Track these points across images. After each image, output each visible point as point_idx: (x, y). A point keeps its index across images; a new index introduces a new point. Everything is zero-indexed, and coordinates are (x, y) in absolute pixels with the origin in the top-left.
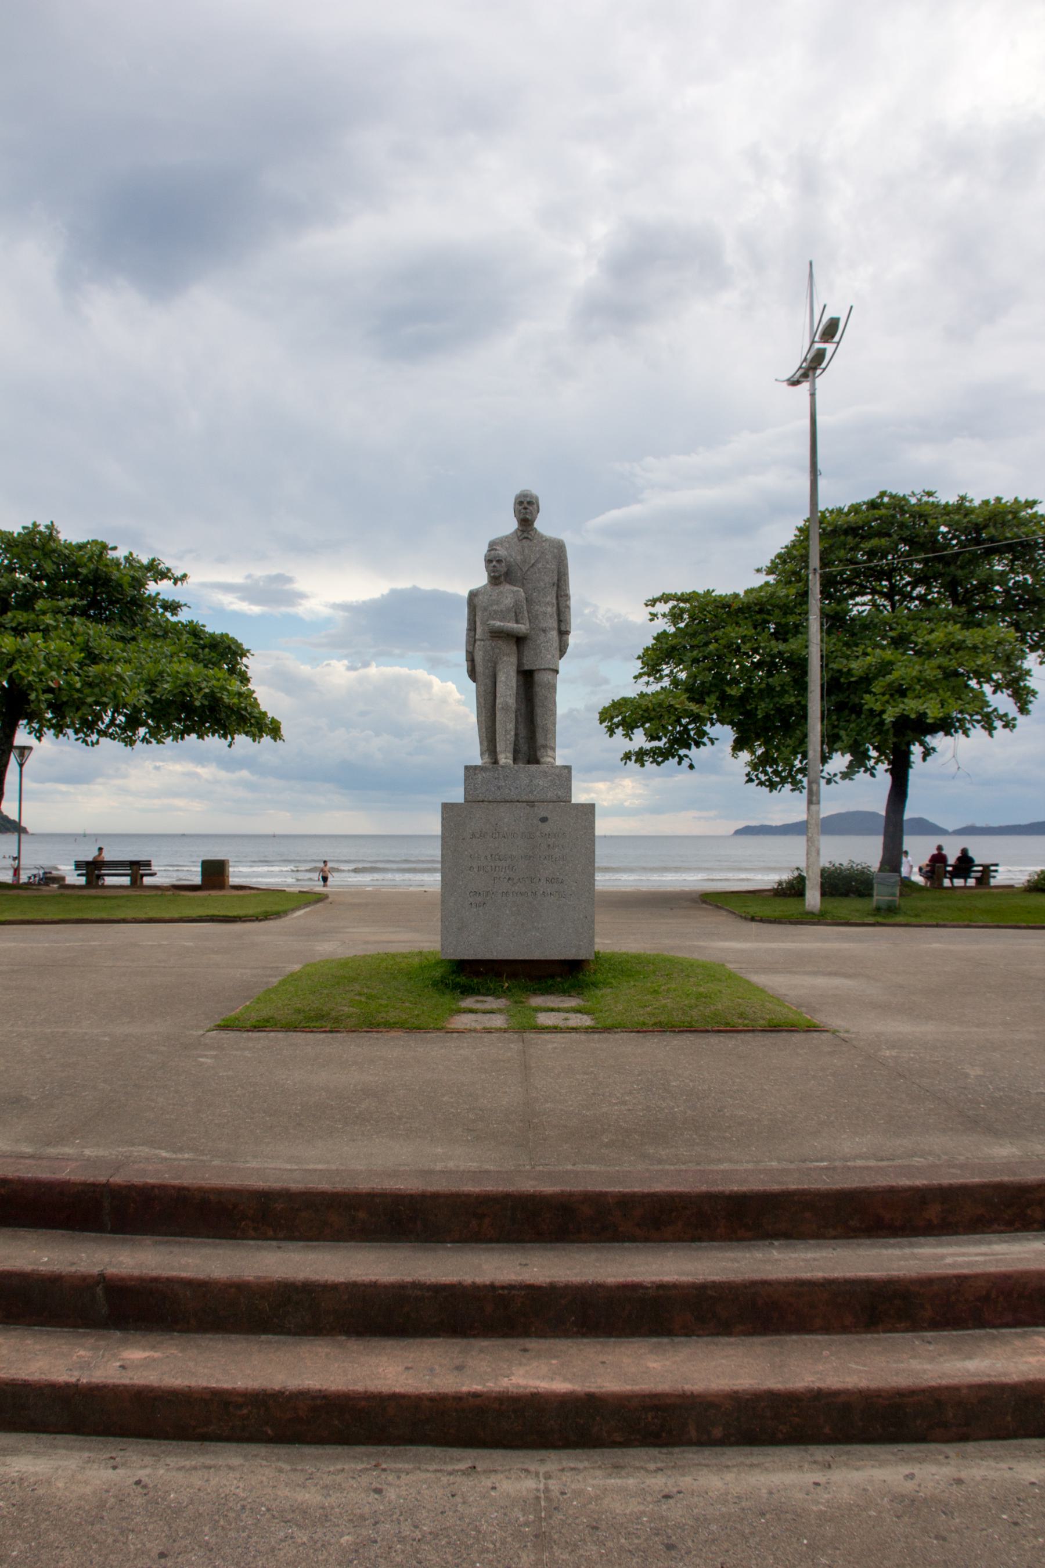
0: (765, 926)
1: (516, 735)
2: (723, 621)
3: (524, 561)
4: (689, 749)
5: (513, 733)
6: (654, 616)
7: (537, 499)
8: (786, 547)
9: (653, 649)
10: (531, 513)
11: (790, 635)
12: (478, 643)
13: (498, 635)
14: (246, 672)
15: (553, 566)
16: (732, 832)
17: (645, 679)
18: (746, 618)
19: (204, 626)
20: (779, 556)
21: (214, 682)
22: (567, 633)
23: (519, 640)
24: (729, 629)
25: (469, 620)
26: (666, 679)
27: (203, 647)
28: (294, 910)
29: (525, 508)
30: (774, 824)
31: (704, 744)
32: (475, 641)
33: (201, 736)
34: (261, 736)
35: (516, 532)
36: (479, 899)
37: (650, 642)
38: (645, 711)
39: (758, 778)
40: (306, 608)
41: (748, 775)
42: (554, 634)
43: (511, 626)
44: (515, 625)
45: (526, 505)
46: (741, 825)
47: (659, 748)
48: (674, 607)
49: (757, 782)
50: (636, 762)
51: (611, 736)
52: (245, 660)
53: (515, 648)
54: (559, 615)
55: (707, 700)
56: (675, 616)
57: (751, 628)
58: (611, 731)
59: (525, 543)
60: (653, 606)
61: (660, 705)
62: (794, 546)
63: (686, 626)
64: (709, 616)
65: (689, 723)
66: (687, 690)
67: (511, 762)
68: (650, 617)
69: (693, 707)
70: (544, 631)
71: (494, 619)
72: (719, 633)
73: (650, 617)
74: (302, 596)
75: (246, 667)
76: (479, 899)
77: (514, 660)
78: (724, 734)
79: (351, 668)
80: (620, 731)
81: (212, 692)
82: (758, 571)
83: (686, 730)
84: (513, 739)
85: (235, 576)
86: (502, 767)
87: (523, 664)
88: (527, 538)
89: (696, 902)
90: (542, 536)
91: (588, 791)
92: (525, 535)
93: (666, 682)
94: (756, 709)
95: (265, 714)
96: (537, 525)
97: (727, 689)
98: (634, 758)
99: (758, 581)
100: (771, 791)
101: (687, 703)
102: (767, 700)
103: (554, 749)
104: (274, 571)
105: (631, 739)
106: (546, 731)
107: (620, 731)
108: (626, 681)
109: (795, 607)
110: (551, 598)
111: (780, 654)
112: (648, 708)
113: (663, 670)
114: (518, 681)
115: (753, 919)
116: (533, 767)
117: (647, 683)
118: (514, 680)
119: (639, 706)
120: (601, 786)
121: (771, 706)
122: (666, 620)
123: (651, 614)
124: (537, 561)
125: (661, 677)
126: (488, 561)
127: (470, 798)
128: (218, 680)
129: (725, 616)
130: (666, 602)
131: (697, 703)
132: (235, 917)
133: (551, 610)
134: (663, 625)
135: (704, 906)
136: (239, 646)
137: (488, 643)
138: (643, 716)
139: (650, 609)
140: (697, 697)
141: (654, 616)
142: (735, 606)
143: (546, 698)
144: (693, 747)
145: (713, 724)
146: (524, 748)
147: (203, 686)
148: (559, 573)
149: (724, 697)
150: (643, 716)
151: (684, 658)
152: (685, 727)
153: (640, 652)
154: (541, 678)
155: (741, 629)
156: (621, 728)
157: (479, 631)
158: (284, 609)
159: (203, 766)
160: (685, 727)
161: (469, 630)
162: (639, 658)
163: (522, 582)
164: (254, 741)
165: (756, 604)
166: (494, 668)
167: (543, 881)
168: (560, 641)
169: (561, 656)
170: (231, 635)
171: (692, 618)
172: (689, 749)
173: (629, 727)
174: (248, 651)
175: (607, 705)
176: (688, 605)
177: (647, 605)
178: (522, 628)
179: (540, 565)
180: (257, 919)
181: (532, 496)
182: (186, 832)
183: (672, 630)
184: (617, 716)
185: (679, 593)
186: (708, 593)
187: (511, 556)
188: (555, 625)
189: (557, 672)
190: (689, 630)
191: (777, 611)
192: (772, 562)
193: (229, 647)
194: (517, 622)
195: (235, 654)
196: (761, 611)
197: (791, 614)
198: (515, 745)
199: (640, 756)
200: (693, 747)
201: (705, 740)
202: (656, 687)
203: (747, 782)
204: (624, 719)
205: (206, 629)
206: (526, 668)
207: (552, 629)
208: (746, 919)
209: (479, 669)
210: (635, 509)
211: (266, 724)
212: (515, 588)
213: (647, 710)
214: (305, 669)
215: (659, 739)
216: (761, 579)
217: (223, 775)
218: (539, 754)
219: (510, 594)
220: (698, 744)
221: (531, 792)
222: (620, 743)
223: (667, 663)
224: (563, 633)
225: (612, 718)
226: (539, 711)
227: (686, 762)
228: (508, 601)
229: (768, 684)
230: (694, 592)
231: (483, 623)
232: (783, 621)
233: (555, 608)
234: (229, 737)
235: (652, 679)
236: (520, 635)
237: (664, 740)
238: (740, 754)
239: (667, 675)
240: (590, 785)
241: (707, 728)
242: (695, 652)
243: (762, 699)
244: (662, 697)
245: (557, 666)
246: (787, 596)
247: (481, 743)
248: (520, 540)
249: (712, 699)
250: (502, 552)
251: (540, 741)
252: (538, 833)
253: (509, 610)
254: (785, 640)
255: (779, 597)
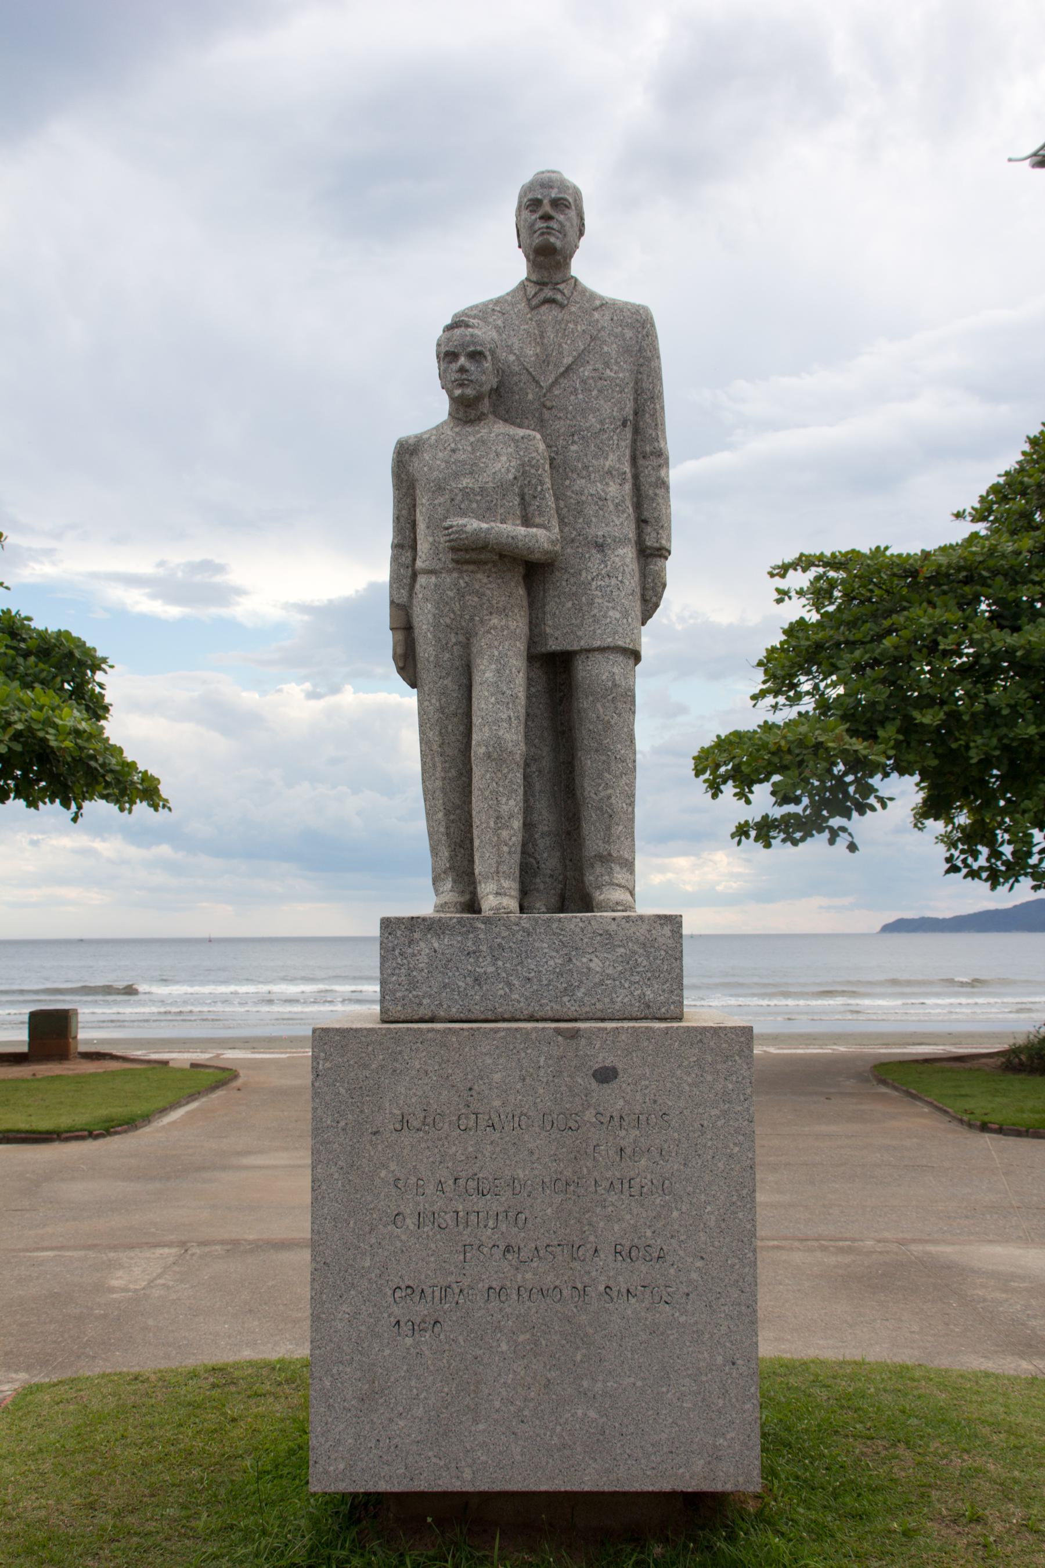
0: (1011, 1141)
1: (528, 826)
2: (904, 598)
3: (545, 361)
4: (849, 818)
5: (517, 824)
6: (783, 595)
7: (577, 194)
8: (1007, 474)
9: (782, 649)
10: (562, 231)
11: (1025, 619)
12: (422, 580)
13: (473, 555)
14: (102, 696)
15: (621, 372)
16: (878, 928)
17: (770, 700)
18: (945, 593)
19: (29, 619)
20: (995, 489)
21: (33, 713)
22: (662, 553)
23: (534, 572)
24: (916, 611)
25: (397, 519)
26: (806, 699)
27: (26, 655)
28: (164, 1111)
29: (546, 217)
30: (940, 915)
31: (873, 809)
32: (414, 576)
33: (32, 804)
34: (132, 802)
35: (522, 286)
36: (421, 1310)
37: (777, 639)
38: (773, 754)
39: (967, 865)
40: (242, 610)
41: (949, 860)
42: (627, 554)
43: (511, 530)
44: (522, 530)
45: (547, 208)
46: (891, 917)
47: (796, 816)
48: (818, 578)
49: (964, 871)
50: (756, 840)
51: (715, 796)
52: (99, 676)
53: (522, 591)
54: (638, 506)
55: (881, 733)
56: (819, 594)
57: (955, 608)
58: (715, 788)
59: (548, 313)
60: (783, 576)
61: (801, 743)
62: (1021, 470)
63: (839, 608)
64: (877, 592)
65: (846, 774)
66: (844, 718)
67: (513, 904)
68: (776, 596)
69: (859, 746)
70: (600, 547)
71: (464, 514)
72: (899, 619)
73: (776, 596)
74: (240, 592)
75: (101, 686)
76: (421, 1310)
77: (518, 623)
78: (904, 791)
79: (312, 695)
80: (729, 789)
81: (29, 729)
82: (959, 515)
83: (841, 784)
84: (517, 840)
85: (141, 562)
86: (487, 921)
87: (544, 636)
88: (551, 301)
89: (867, 1081)
90: (593, 296)
91: (662, 869)
92: (548, 293)
93: (808, 705)
94: (967, 747)
95: (132, 766)
96: (580, 267)
97: (916, 714)
98: (753, 833)
99: (960, 532)
100: (993, 888)
101: (847, 738)
102: (986, 732)
103: (629, 866)
104: (198, 557)
105: (748, 802)
106: (609, 816)
107: (729, 789)
108: (738, 704)
109: (1029, 569)
110: (618, 459)
111: (1009, 653)
112: (779, 749)
113: (797, 685)
114: (530, 682)
115: (984, 1128)
116: (573, 920)
117: (775, 707)
118: (520, 680)
119: (764, 746)
120: (682, 862)
121: (994, 741)
122: (803, 601)
123: (778, 590)
124: (580, 359)
125: (799, 696)
126: (447, 356)
127: (396, 1011)
128: (41, 709)
129: (905, 591)
130: (804, 570)
131: (864, 740)
132: (48, 1132)
133: (618, 491)
134: (799, 610)
135: (884, 1089)
136: (89, 652)
137: (448, 579)
138: (770, 762)
139: (779, 583)
140: (863, 728)
141: (783, 595)
142: (927, 572)
143: (608, 726)
144: (855, 814)
145: (886, 775)
146: (550, 861)
147: (13, 719)
148: (638, 392)
149: (909, 728)
150: (770, 762)
151: (840, 663)
152: (840, 779)
153: (762, 654)
154: (596, 671)
155: (938, 612)
156: (730, 783)
157: (423, 546)
158: (214, 611)
159: (104, 840)
160: (840, 779)
161: (397, 546)
162: (760, 664)
163: (539, 416)
164: (122, 810)
165: (959, 569)
166: (467, 646)
167: (606, 1254)
168: (644, 574)
169: (646, 616)
170: (74, 634)
171: (849, 597)
172: (849, 818)
173: (745, 781)
174: (104, 660)
175: (706, 745)
176: (842, 575)
177: (772, 575)
178: (541, 538)
179: (586, 372)
180: (89, 1134)
181: (563, 185)
182: (84, 937)
183: (814, 617)
184: (726, 764)
185: (828, 554)
186: (878, 552)
187: (510, 349)
188: (630, 531)
189: (636, 656)
190: (846, 616)
191: (999, 579)
192: (983, 499)
193: (71, 654)
194: (526, 522)
195: (81, 665)
196: (967, 581)
197: (1024, 583)
198: (524, 852)
199: (764, 831)
200: (855, 814)
201: (872, 800)
202: (790, 713)
203: (948, 872)
204: (737, 769)
205: (33, 624)
206: (553, 646)
207: (621, 542)
208: (970, 1125)
209: (426, 650)
210: (723, 459)
211: (133, 783)
212: (521, 432)
213: (778, 751)
214: (250, 698)
215: (797, 801)
216: (964, 530)
217: (132, 851)
218: (589, 878)
219: (504, 449)
220: (862, 809)
221: (569, 990)
222: (731, 807)
223: (808, 673)
224: (651, 554)
225: (718, 766)
226: (588, 763)
227: (843, 840)
228: (501, 465)
229: (987, 704)
230: (853, 551)
231: (434, 525)
232: (1011, 595)
233: (628, 487)
234: (73, 806)
235: (781, 699)
236: (536, 556)
237: (805, 801)
238: (930, 822)
239: (808, 693)
240: (667, 861)
241: (876, 781)
242: (857, 653)
243: (976, 729)
244: (803, 729)
245: (637, 640)
246: (1018, 553)
247: (434, 851)
248: (533, 308)
249: (889, 732)
250: (484, 333)
251: (593, 844)
252: (589, 1115)
253: (503, 488)
254: (1016, 629)
255: (1003, 556)
